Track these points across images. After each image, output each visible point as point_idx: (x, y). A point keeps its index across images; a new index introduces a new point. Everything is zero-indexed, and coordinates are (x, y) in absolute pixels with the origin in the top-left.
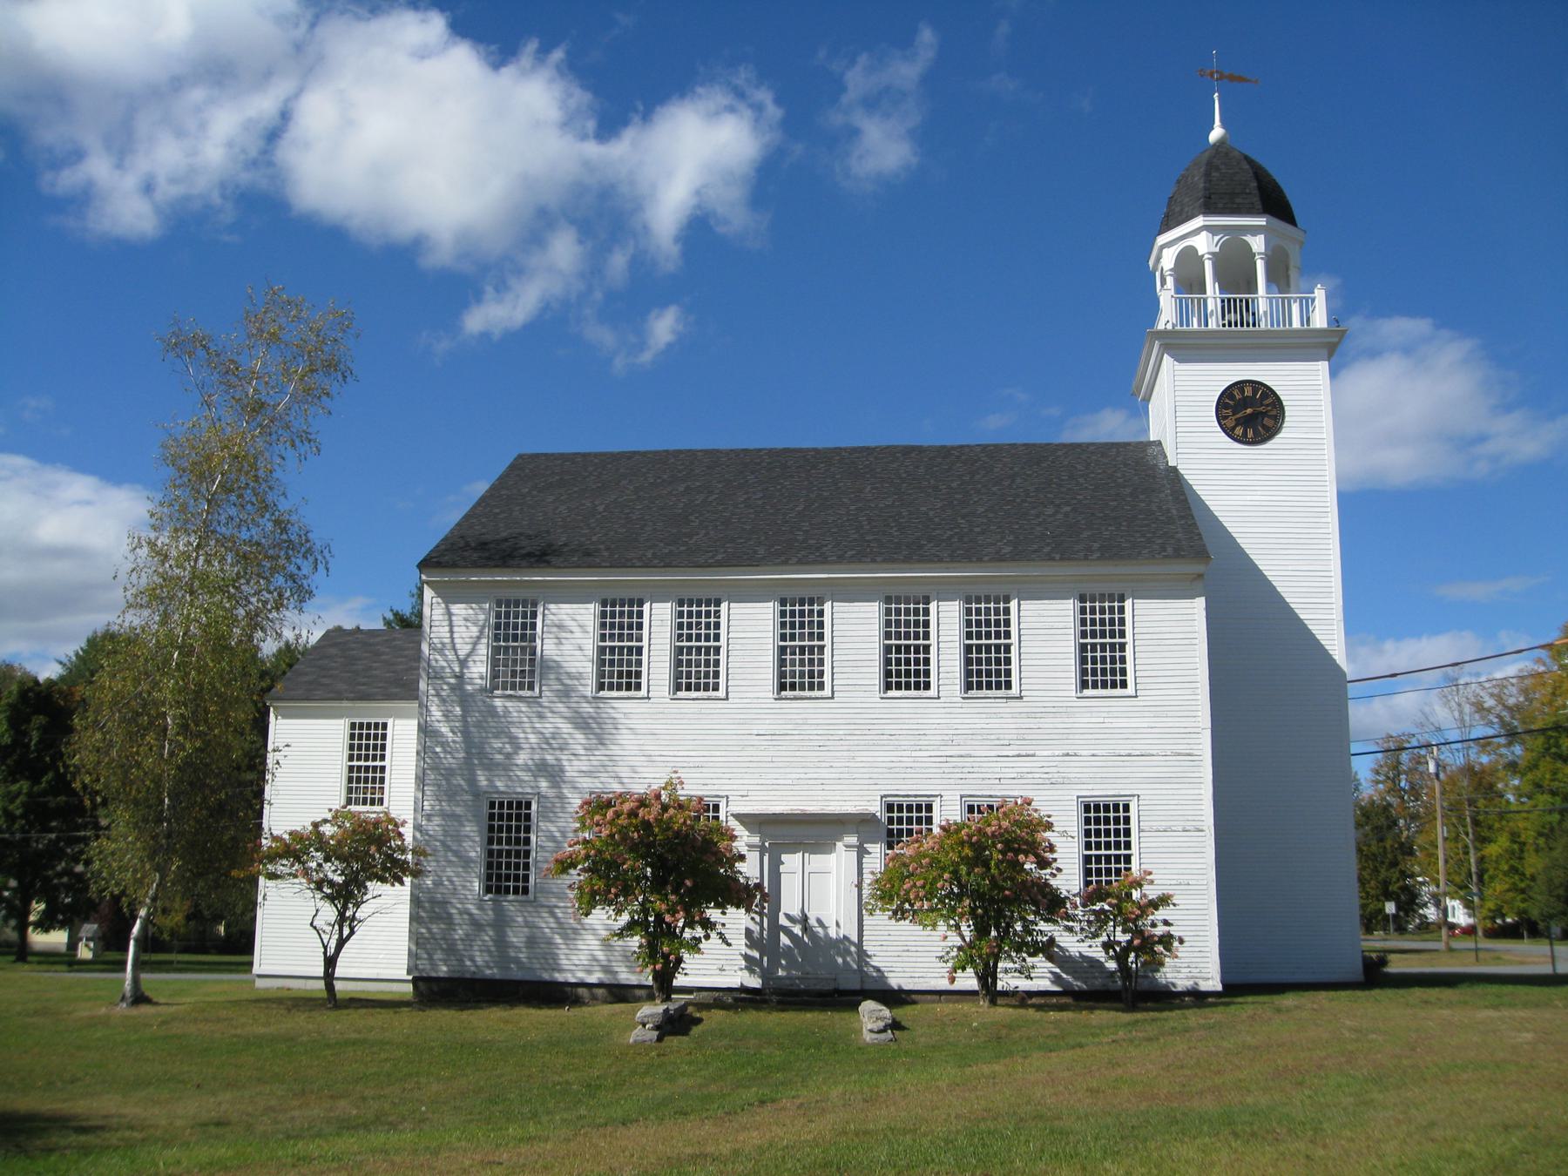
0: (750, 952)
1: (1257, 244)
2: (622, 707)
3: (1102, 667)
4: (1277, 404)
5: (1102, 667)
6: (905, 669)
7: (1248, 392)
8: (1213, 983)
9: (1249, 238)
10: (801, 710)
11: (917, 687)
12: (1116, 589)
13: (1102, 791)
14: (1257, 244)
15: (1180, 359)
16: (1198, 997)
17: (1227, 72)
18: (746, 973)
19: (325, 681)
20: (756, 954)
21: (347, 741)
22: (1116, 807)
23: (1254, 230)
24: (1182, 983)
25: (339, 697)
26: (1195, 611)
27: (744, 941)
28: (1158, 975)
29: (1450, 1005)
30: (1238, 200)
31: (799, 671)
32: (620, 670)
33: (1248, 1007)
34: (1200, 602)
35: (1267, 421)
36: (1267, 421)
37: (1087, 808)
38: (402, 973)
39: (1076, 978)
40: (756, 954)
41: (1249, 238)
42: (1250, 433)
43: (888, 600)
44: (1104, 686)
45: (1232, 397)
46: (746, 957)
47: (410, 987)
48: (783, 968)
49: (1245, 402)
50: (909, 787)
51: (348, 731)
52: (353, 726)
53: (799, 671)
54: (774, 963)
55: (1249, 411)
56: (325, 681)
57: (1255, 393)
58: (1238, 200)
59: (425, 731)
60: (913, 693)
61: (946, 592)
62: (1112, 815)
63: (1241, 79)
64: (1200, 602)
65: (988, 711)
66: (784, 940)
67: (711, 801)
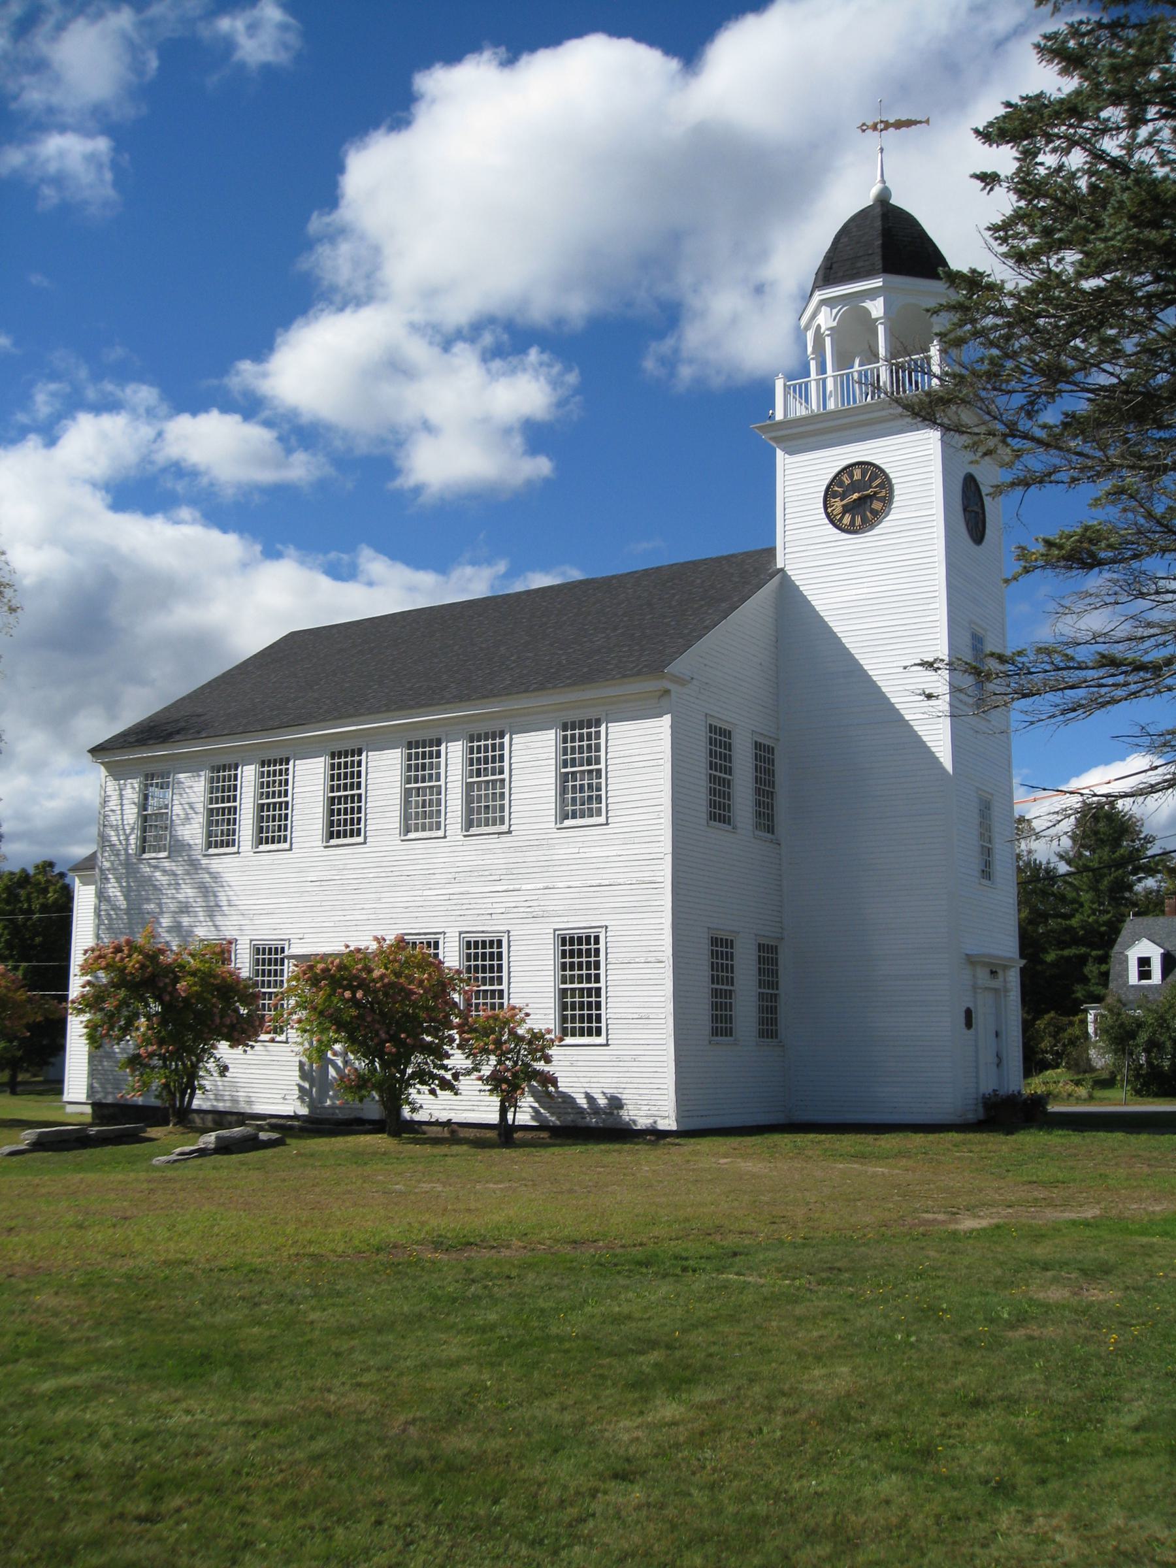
0: (302, 1083)
1: (876, 308)
2: (224, 864)
3: (580, 794)
4: (887, 483)
5: (580, 794)
6: (420, 813)
7: (857, 475)
8: (669, 1123)
9: (868, 304)
10: (346, 854)
12: (592, 714)
13: (576, 923)
14: (876, 308)
15: (791, 452)
16: (656, 1135)
17: (892, 121)
18: (298, 1103)
20: (307, 1085)
22: (588, 938)
23: (871, 294)
24: (643, 1123)
26: (660, 729)
27: (298, 1073)
28: (622, 1112)
29: (861, 1157)
30: (859, 264)
32: (221, 834)
33: (692, 1144)
34: (667, 720)
35: (877, 505)
36: (877, 505)
37: (469, 947)
38: (83, 1097)
39: (552, 1114)
40: (307, 1085)
41: (868, 304)
42: (847, 519)
43: (410, 746)
46: (301, 1088)
47: (88, 1109)
48: (332, 1098)
49: (854, 487)
50: (414, 925)
53: (343, 820)
54: (323, 1094)
55: (855, 496)
57: (864, 474)
58: (859, 264)
59: (101, 896)
61: (381, 742)
63: (909, 123)
64: (667, 720)
65: (486, 850)
66: (332, 1072)
67: (592, 932)
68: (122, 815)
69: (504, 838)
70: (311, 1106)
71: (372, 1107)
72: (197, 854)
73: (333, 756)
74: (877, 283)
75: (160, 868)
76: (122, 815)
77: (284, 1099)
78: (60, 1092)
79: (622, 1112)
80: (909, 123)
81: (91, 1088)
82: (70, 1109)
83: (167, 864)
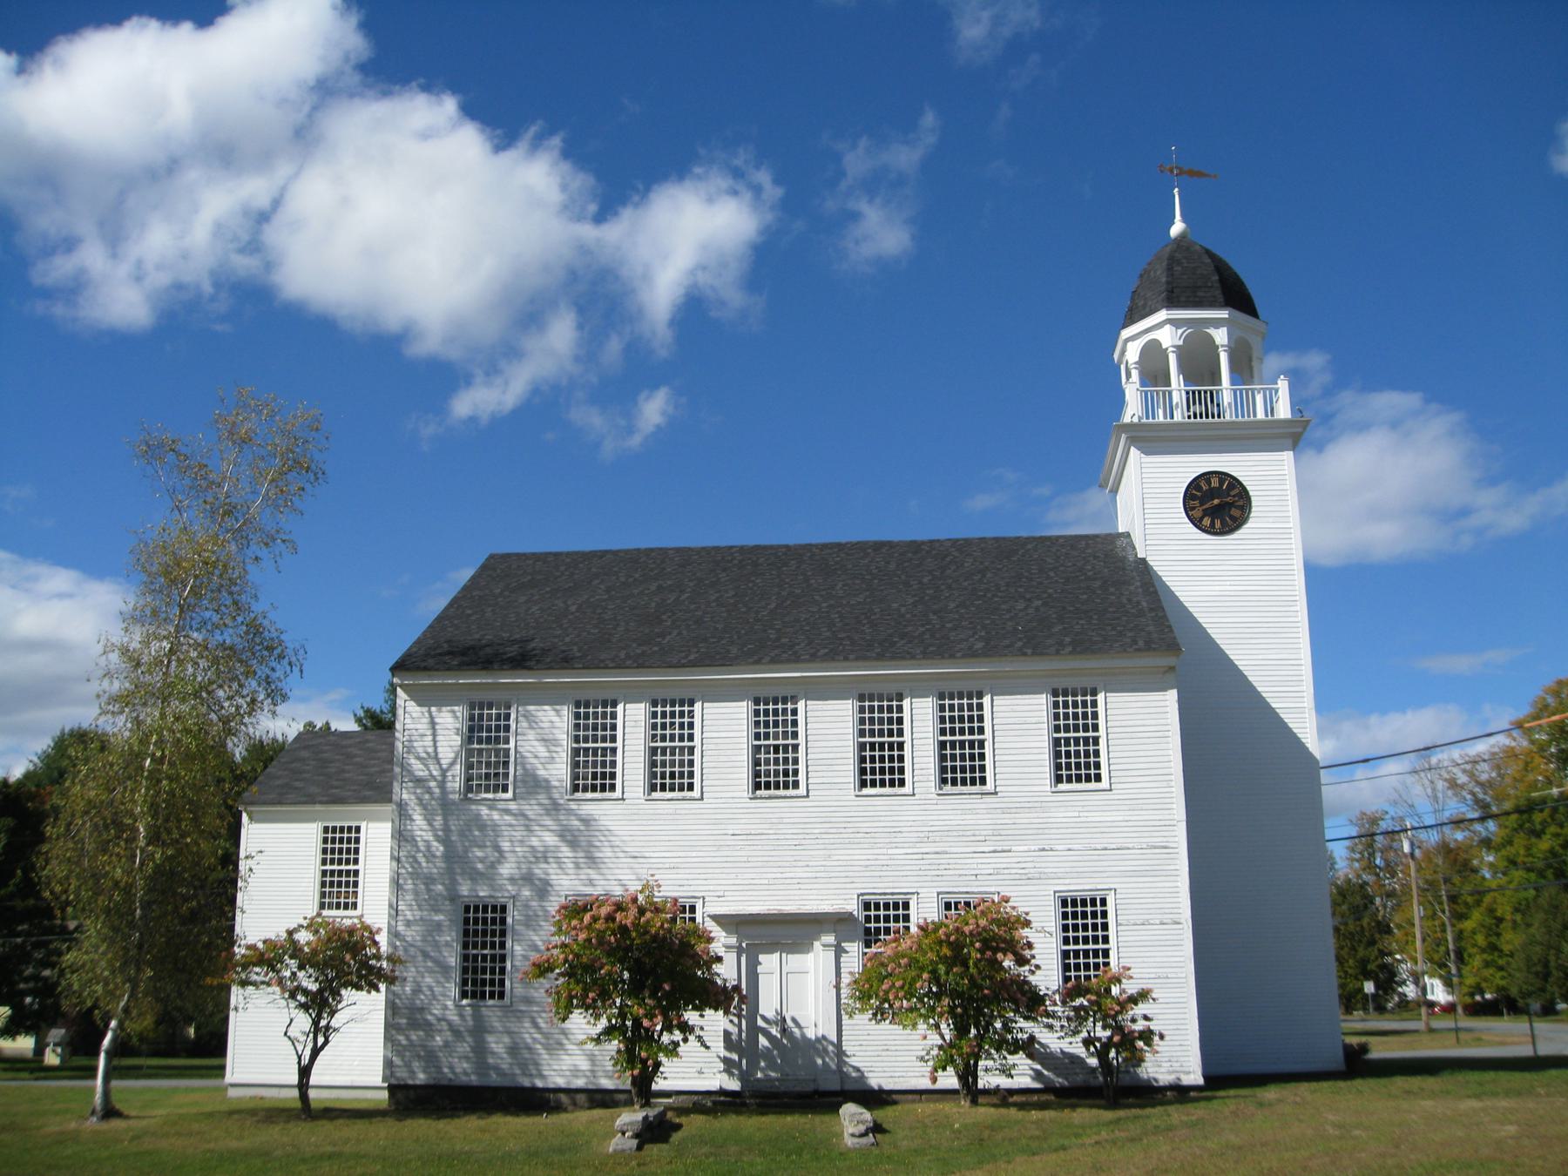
0: (728, 1055)
1: (1220, 336)
3: (1075, 761)
4: (1244, 495)
5: (1075, 761)
6: (879, 766)
8: (1195, 1077)
10: (777, 809)
11: (892, 784)
12: (1088, 683)
13: (1080, 886)
14: (1220, 336)
15: (1147, 452)
16: (1181, 1092)
18: (725, 1076)
19: (297, 784)
20: (735, 1057)
21: (320, 846)
23: (1217, 323)
25: (311, 800)
28: (1139, 1070)
30: (1200, 294)
31: (774, 771)
40: (735, 1057)
42: (1218, 524)
43: (861, 698)
44: (1079, 779)
45: (1199, 488)
46: (726, 1060)
47: (385, 1095)
48: (762, 1070)
49: (1212, 493)
51: (321, 835)
52: (326, 830)
53: (774, 771)
54: (753, 1065)
55: (1216, 502)
56: (297, 784)
59: (401, 836)
60: (887, 790)
62: (1089, 909)
63: (1200, 174)
65: (963, 807)
66: (763, 1041)
68: (435, 741)
69: (988, 799)
70: (743, 1078)
71: (948, 1079)
72: (561, 796)
73: (757, 702)
74: (1223, 314)
75: (496, 810)
76: (435, 741)
77: (700, 1072)
78: (223, 1076)
79: (1139, 1070)
80: (1200, 174)
81: (388, 1064)
82: (232, 1093)
83: (513, 806)
